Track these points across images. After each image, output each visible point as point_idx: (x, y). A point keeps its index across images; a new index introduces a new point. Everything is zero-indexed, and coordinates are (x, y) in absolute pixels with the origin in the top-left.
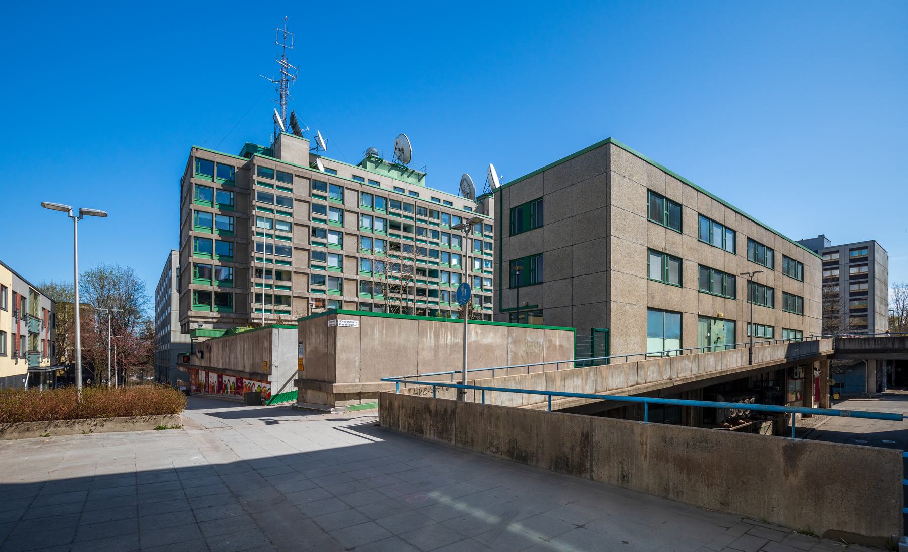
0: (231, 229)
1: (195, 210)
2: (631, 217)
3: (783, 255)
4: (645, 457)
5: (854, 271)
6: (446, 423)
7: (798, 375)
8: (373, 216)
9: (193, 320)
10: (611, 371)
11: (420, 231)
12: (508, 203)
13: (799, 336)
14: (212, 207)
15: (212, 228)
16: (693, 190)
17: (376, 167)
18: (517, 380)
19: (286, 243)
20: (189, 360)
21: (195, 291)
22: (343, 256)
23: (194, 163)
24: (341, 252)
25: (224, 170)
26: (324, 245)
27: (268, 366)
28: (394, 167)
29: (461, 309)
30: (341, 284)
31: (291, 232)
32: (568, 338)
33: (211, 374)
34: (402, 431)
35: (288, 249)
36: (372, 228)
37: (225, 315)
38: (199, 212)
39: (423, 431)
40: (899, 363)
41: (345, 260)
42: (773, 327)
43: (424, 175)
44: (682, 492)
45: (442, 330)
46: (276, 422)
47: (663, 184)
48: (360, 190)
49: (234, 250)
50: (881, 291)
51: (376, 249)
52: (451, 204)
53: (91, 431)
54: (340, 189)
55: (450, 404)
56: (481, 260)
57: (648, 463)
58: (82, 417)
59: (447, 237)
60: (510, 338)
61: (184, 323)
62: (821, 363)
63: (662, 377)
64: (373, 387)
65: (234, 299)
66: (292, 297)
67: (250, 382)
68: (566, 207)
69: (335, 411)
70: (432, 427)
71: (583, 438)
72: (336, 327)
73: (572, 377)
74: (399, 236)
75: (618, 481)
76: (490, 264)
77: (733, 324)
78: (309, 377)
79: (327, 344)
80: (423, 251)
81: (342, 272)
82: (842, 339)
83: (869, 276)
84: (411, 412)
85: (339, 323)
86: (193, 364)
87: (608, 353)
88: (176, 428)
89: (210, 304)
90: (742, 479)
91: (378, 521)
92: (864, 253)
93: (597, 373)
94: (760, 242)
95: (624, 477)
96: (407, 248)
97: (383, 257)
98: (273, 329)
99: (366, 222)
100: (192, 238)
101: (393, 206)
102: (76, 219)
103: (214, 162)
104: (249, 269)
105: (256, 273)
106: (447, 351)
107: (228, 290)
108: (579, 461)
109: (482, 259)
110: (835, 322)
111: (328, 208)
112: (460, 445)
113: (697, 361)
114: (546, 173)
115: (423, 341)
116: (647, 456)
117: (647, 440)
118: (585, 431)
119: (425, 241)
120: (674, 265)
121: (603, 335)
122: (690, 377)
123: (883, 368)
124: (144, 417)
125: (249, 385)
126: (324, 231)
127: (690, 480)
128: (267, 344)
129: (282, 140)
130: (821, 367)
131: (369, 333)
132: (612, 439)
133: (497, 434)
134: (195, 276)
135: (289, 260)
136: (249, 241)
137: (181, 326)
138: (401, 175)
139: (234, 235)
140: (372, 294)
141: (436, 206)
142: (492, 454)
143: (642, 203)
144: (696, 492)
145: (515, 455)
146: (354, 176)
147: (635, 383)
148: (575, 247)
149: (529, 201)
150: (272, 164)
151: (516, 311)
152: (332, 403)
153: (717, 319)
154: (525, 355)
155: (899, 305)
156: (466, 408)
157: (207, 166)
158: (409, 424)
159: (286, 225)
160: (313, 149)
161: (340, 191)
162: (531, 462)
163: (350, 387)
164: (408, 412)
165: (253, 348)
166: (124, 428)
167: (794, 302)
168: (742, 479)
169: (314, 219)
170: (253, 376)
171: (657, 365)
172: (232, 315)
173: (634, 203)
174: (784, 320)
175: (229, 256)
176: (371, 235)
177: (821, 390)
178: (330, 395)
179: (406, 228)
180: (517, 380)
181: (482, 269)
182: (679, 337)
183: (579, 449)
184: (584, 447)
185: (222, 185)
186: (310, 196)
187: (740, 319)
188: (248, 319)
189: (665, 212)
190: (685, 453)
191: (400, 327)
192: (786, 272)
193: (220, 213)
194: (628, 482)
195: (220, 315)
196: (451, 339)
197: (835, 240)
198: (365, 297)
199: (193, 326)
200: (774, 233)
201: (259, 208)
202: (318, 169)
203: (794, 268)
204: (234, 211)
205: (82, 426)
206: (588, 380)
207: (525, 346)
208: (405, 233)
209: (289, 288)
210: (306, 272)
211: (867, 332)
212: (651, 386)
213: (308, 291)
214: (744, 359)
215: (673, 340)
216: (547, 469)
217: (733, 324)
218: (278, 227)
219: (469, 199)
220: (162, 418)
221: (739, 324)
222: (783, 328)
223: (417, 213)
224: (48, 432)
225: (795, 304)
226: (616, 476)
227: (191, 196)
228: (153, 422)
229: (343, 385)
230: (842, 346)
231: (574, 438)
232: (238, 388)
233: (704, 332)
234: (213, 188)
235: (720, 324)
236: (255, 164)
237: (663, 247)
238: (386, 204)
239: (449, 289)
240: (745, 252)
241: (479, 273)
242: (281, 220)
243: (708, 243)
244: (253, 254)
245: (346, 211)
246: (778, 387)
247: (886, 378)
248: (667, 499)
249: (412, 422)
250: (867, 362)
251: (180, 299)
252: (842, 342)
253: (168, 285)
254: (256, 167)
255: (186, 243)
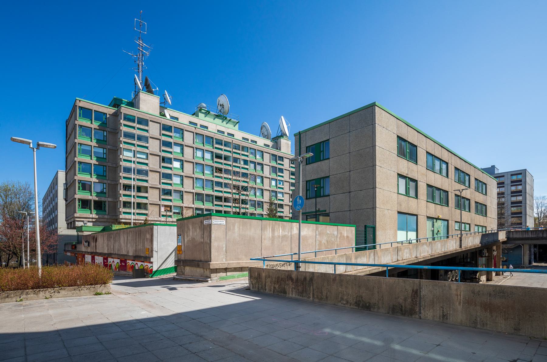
0: (105, 157)
1: (78, 143)
2: (388, 154)
3: (475, 178)
4: (460, 303)
5: (513, 188)
6: (306, 286)
7: (485, 254)
8: (203, 150)
9: (78, 219)
10: (383, 253)
11: (236, 160)
12: (305, 143)
13: (484, 230)
14: (91, 141)
15: (91, 156)
16: (423, 136)
17: (205, 116)
18: (330, 259)
19: (144, 167)
20: (76, 247)
21: (79, 200)
22: (184, 176)
23: (78, 110)
24: (182, 174)
25: (99, 115)
26: (171, 168)
27: (150, 251)
28: (217, 116)
29: (268, 212)
30: (182, 195)
31: (148, 160)
32: (352, 231)
33: (96, 257)
34: (269, 292)
35: (145, 171)
36: (203, 158)
37: (101, 216)
38: (82, 145)
39: (286, 292)
40: (541, 246)
41: (185, 179)
42: (470, 224)
43: (237, 123)
44: (487, 324)
45: (276, 227)
46: (175, 289)
47: (406, 133)
48: (195, 131)
49: (107, 171)
50: (530, 201)
51: (206, 172)
52: (256, 142)
53: (51, 297)
54: (181, 131)
55: (308, 275)
56: (276, 180)
57: (461, 307)
58: (44, 287)
59: (253, 164)
60: (317, 231)
61: (70, 222)
62: (497, 247)
63: (411, 256)
64: (234, 264)
65: (107, 205)
66: (148, 204)
67: (134, 262)
68: (345, 146)
69: (211, 280)
70: (293, 289)
71: (413, 293)
72: (211, 224)
73: (361, 256)
74: (221, 163)
75: (440, 318)
76: (282, 182)
77: (447, 222)
78: (186, 258)
79: (203, 236)
80: (236, 173)
81: (183, 187)
82: (511, 231)
83: (523, 192)
84: (276, 280)
85: (213, 222)
86: (79, 250)
87: (374, 242)
88: (108, 294)
89: (90, 209)
90: (529, 314)
91: (310, 347)
92: (520, 177)
93: (375, 253)
94: (462, 170)
95: (444, 316)
96: (227, 171)
97: (210, 178)
98: (154, 226)
99: (199, 154)
100: (77, 163)
101: (217, 143)
102: (35, 150)
103: (92, 110)
104: (118, 184)
105: (123, 187)
106: (279, 240)
107: (103, 199)
108: (411, 307)
109: (276, 179)
110: (503, 221)
111: (173, 144)
112: (316, 300)
113: (431, 245)
114: (331, 124)
115: (265, 234)
116: (461, 303)
117: (461, 293)
118: (415, 288)
119: (239, 167)
120: (412, 184)
121: (372, 229)
122: (427, 256)
123: (532, 249)
124: (86, 286)
125: (133, 264)
126: (171, 159)
127: (492, 316)
128: (148, 236)
129: (140, 96)
130: (497, 249)
131: (232, 228)
132: (435, 293)
133: (347, 293)
134: (79, 189)
135: (146, 178)
136: (117, 165)
137: (68, 224)
138: (222, 122)
139: (107, 161)
140: (203, 202)
141: (246, 143)
142: (343, 305)
143: (394, 145)
144: (497, 323)
145: (361, 305)
146: (190, 122)
147: (397, 260)
148: (351, 172)
149: (320, 142)
150: (134, 113)
151: (315, 214)
152: (208, 275)
153: (437, 219)
154: (326, 243)
155: (538, 210)
156: (322, 277)
157: (87, 113)
158: (275, 288)
159: (144, 155)
160: (162, 103)
161: (181, 132)
162: (373, 309)
163: (220, 265)
164: (274, 280)
165: (136, 239)
166: (73, 294)
167: (482, 208)
168: (529, 314)
169: (163, 151)
170: (136, 258)
171: (409, 248)
172: (106, 217)
173: (389, 145)
174: (476, 220)
175: (103, 176)
176: (202, 162)
177: (497, 264)
178: (206, 270)
179: (226, 158)
180: (330, 259)
181: (276, 186)
182: (416, 230)
183: (411, 300)
184: (414, 299)
185: (98, 126)
186: (160, 135)
187: (451, 219)
188: (117, 219)
189: (407, 150)
190: (489, 300)
191: (251, 224)
192: (477, 189)
193: (97, 146)
194: (447, 319)
195: (98, 216)
196: (282, 232)
197: (501, 169)
198: (199, 205)
199: (78, 224)
200: (470, 164)
201: (125, 142)
202: (166, 117)
203: (481, 186)
204: (107, 145)
205: (45, 293)
206: (370, 259)
207: (326, 237)
208: (225, 161)
209: (147, 198)
210: (158, 187)
211: (522, 227)
212: (406, 262)
213: (160, 200)
214: (457, 244)
215: (412, 232)
216: (386, 313)
217: (447, 222)
218: (138, 156)
219: (267, 139)
220: (99, 287)
221: (450, 222)
222: (475, 225)
223: (234, 148)
224: (21, 298)
225: (482, 209)
226: (438, 315)
227: (75, 133)
228: (92, 289)
229: (216, 263)
230: (511, 236)
231: (406, 293)
232: (123, 266)
233: (430, 228)
234: (92, 128)
235: (439, 221)
236: (121, 113)
237: (406, 173)
238: (213, 142)
239: (255, 199)
240: (453, 176)
241: (275, 189)
242: (140, 151)
243: (432, 170)
244: (121, 174)
245: (186, 146)
246: (473, 262)
247: (533, 256)
248: (475, 328)
249: (277, 286)
250: (523, 246)
251: (66, 205)
252: (511, 233)
253: (55, 196)
254: (123, 114)
255: (71, 166)
